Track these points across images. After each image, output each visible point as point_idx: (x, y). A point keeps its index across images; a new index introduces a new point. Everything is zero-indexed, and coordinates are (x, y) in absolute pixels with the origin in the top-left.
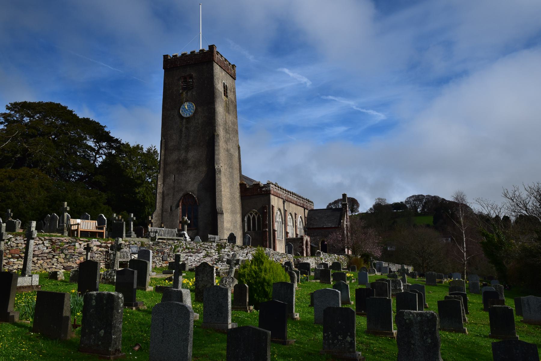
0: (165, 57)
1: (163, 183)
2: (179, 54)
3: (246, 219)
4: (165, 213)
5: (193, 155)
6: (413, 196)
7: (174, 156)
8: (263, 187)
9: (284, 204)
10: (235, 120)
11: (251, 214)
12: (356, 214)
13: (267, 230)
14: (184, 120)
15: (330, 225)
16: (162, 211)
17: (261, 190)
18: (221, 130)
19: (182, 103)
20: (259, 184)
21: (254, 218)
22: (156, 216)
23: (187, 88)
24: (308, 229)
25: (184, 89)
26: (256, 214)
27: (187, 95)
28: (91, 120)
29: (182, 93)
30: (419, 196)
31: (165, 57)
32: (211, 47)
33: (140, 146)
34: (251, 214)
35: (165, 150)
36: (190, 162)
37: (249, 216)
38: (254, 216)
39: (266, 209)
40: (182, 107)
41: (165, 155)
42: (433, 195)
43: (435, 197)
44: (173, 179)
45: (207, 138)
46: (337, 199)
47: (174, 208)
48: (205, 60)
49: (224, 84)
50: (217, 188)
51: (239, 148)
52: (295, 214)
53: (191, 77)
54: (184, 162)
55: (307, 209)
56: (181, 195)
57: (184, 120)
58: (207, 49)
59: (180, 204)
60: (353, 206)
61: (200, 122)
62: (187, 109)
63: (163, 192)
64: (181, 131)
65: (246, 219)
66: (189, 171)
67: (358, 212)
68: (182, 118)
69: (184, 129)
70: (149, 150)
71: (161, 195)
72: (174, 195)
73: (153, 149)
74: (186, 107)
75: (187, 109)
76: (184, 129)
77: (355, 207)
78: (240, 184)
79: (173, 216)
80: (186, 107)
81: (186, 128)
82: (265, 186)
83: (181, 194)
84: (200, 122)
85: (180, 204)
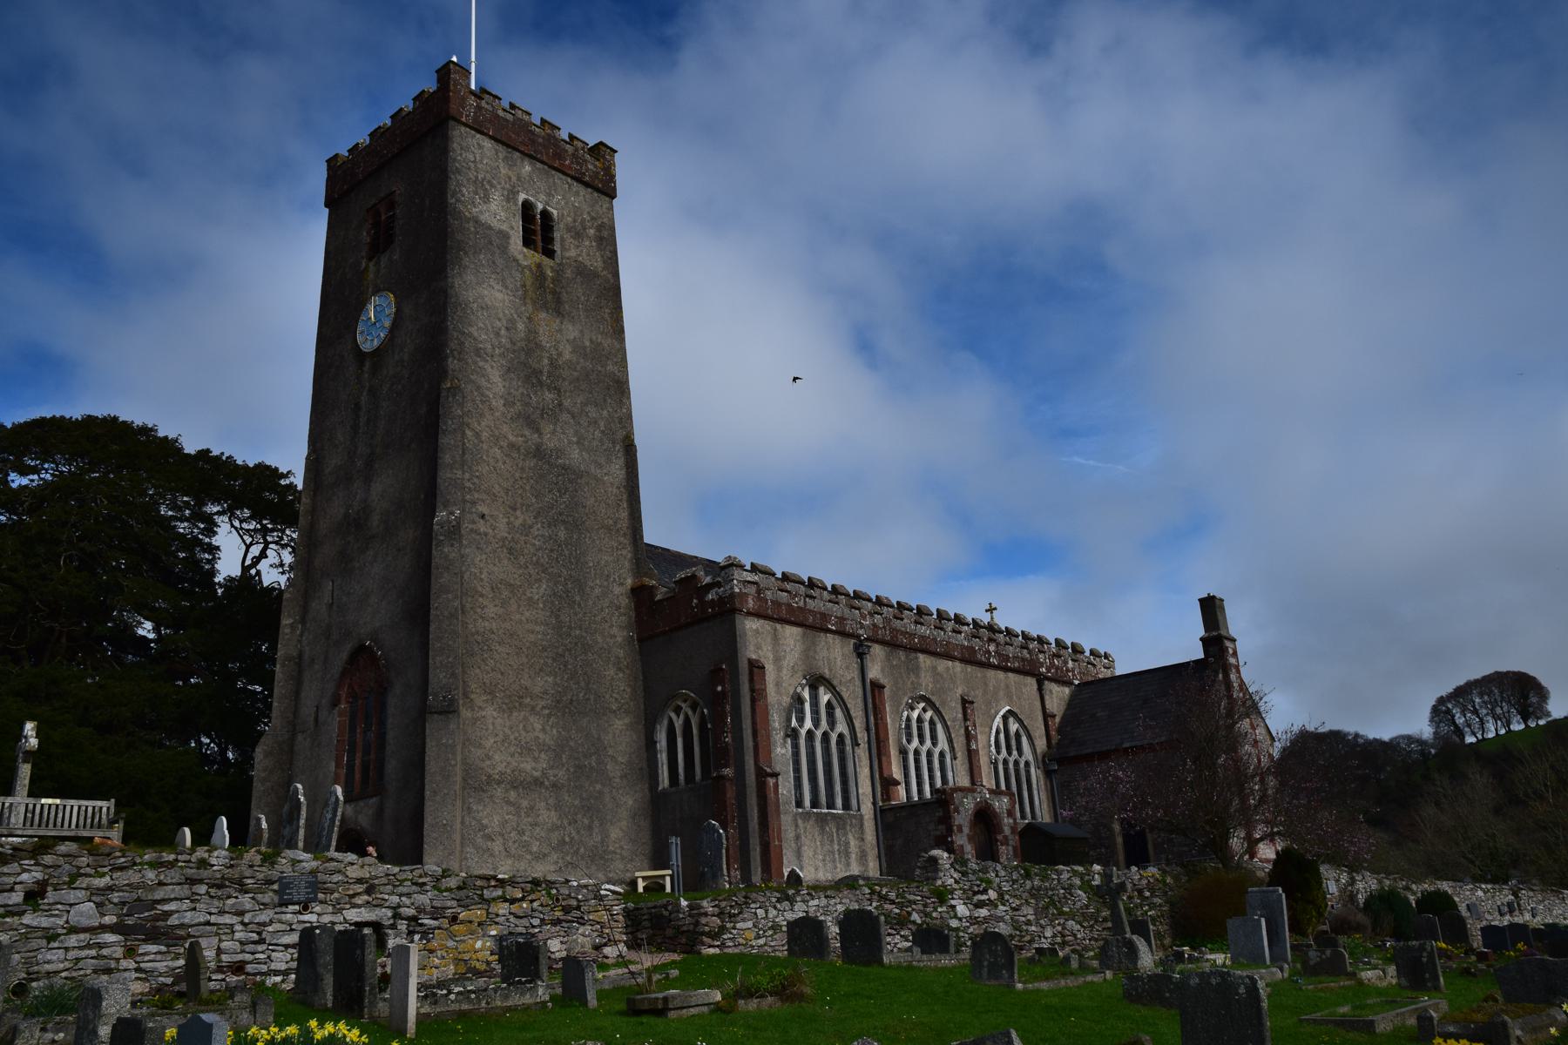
3: (662, 738)
9: (861, 656)
10: (607, 342)
12: (1542, 722)
13: (728, 771)
18: (495, 375)
21: (687, 722)
22: (267, 755)
24: (1060, 761)
28: (190, 448)
29: (366, 268)
34: (678, 710)
37: (671, 720)
46: (1462, 683)
49: (527, 207)
50: (434, 604)
51: (630, 449)
52: (965, 703)
55: (1063, 681)
57: (368, 364)
60: (1526, 697)
64: (357, 407)
65: (662, 738)
67: (1548, 714)
68: (361, 356)
69: (364, 399)
76: (364, 399)
77: (1534, 700)
83: (348, 647)
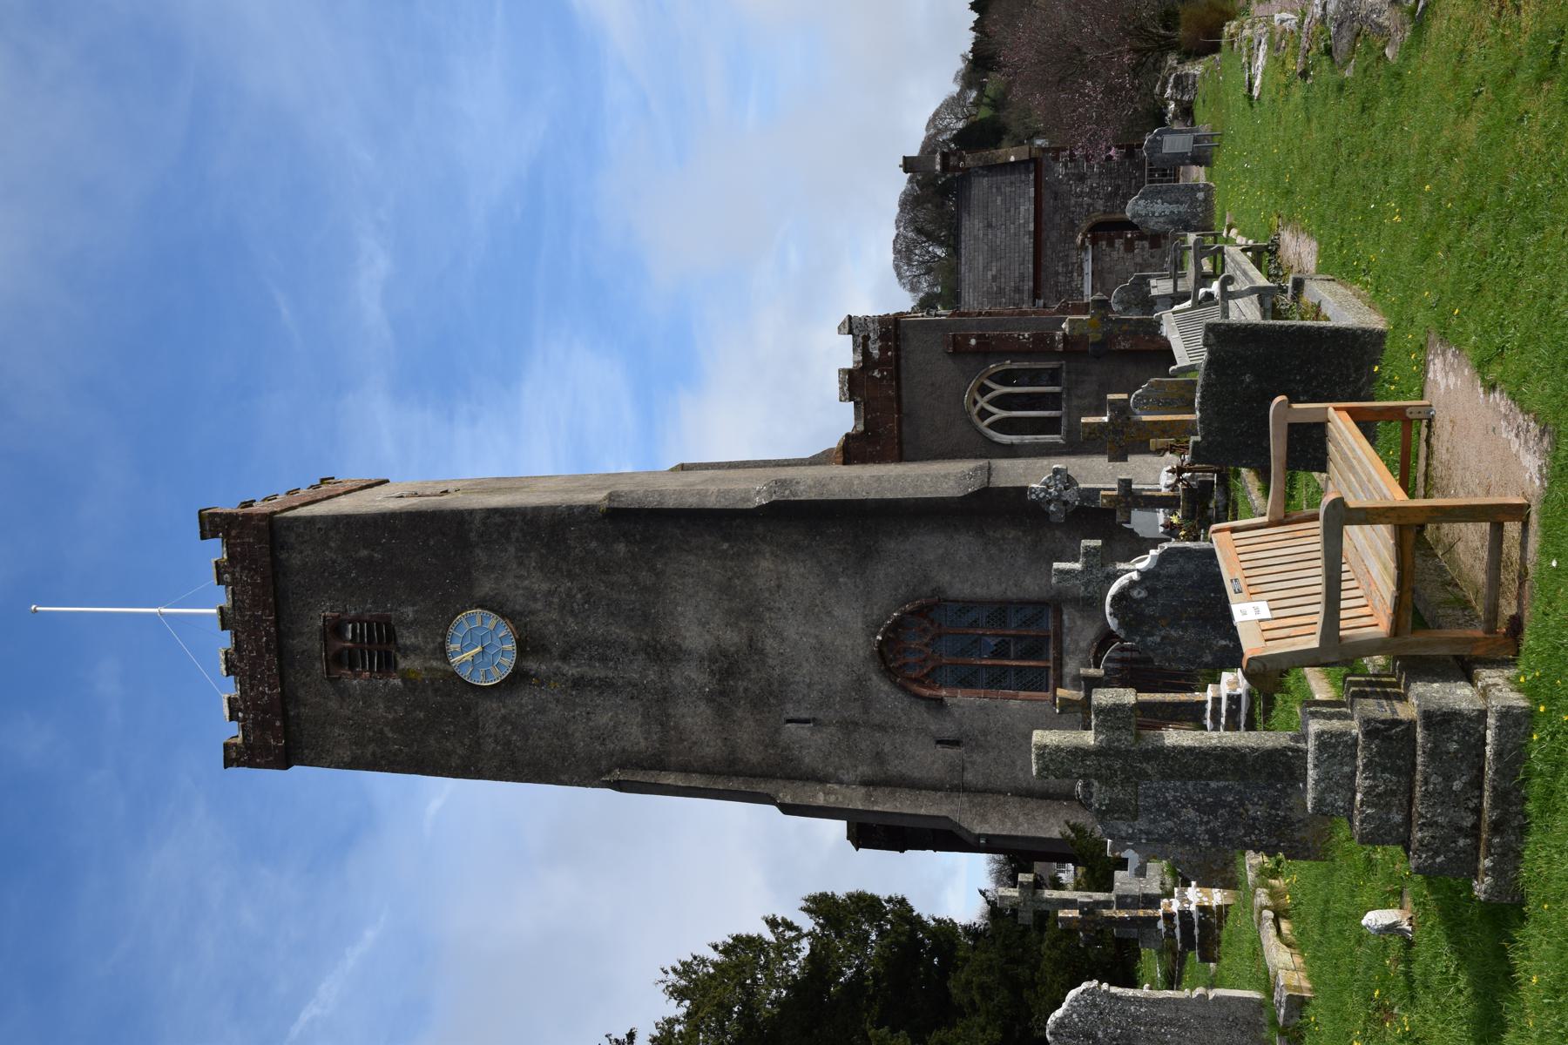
0: (234, 757)
1: (823, 780)
2: (230, 688)
3: (1006, 439)
4: (969, 776)
5: (697, 625)
6: (897, 267)
7: (694, 719)
8: (866, 354)
11: (984, 414)
14: (532, 665)
15: (1026, 209)
16: (962, 788)
17: (878, 364)
19: (453, 679)
20: (850, 372)
21: (1002, 402)
23: (381, 646)
25: (387, 664)
26: (984, 390)
27: (415, 649)
30: (897, 251)
31: (234, 757)
32: (211, 525)
33: (657, 1033)
34: (984, 414)
35: (662, 767)
36: (732, 638)
37: (990, 426)
38: (990, 402)
39: (967, 338)
40: (465, 674)
41: (685, 769)
42: (898, 210)
43: (903, 204)
44: (803, 731)
45: (621, 548)
47: (950, 729)
48: (267, 558)
50: (862, 495)
53: (335, 629)
54: (727, 668)
56: (885, 687)
57: (532, 665)
58: (216, 549)
59: (927, 692)
61: (545, 586)
62: (480, 648)
63: (867, 783)
64: (578, 683)
65: (1006, 439)
66: (770, 644)
68: (518, 677)
69: (571, 670)
70: (678, 993)
71: (878, 793)
72: (881, 728)
73: (672, 977)
74: (468, 655)
75: (480, 648)
76: (571, 670)
78: (844, 463)
79: (985, 733)
80: (468, 655)
81: (565, 657)
82: (862, 346)
83: (880, 686)
84: (545, 586)
85: (927, 692)
